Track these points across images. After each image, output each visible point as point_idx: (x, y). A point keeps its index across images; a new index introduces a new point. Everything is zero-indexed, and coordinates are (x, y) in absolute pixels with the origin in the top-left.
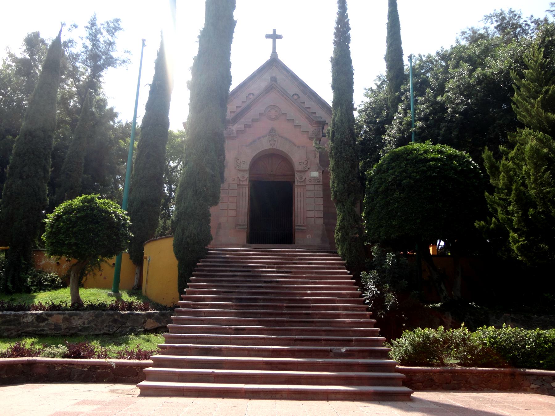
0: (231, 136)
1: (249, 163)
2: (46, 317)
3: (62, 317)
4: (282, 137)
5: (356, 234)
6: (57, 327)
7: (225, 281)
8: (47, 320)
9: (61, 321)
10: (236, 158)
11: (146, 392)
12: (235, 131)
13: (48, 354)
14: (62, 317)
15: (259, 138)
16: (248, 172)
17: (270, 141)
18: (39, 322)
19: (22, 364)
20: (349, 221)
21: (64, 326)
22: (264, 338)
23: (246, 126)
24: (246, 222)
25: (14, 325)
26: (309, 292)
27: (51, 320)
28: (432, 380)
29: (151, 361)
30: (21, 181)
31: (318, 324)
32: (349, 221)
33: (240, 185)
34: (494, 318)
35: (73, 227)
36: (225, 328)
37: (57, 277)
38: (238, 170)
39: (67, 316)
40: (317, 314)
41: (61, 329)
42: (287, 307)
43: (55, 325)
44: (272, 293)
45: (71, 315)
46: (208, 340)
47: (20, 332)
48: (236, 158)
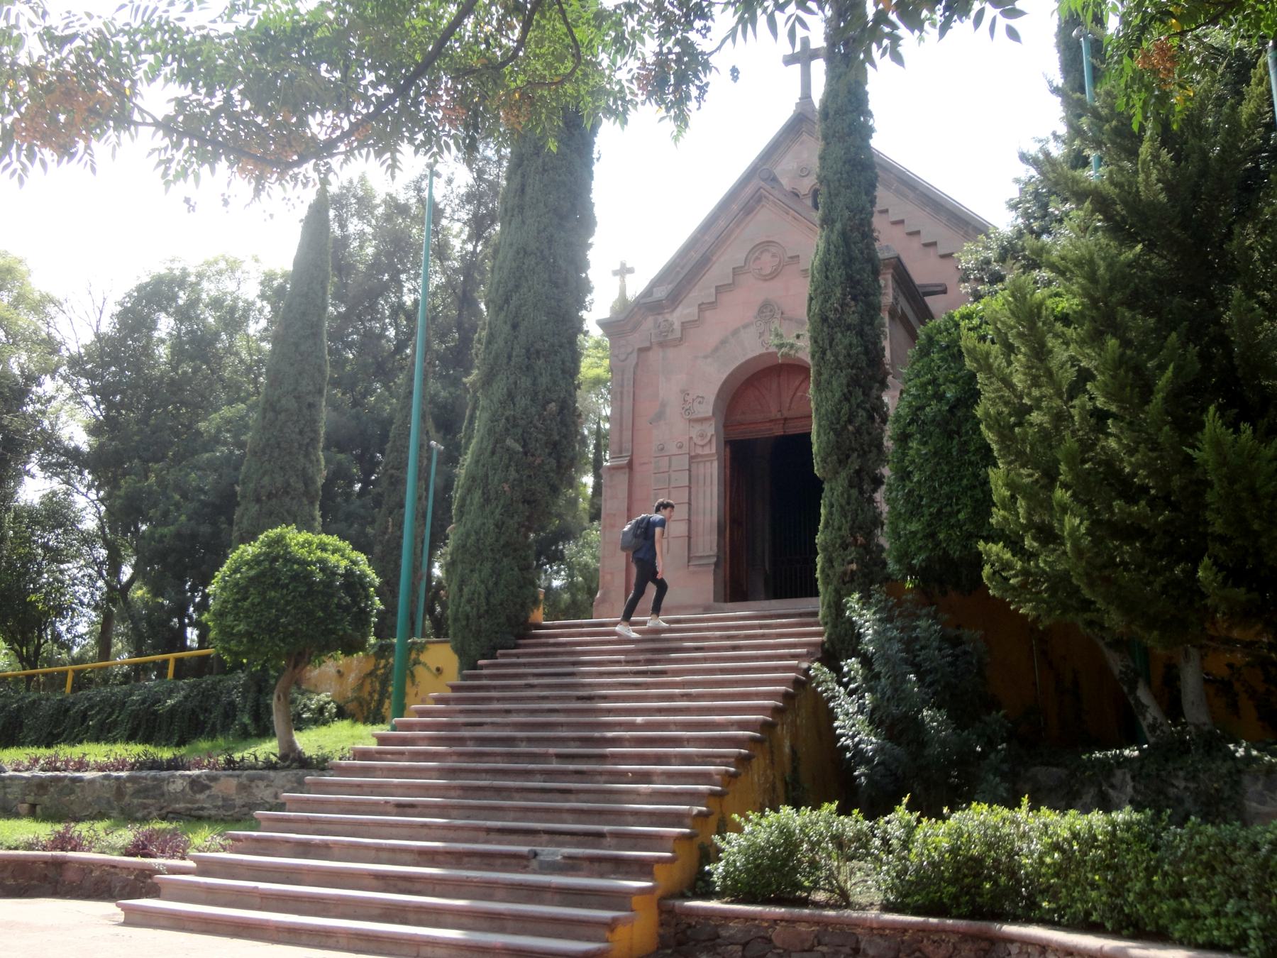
0: (670, 337)
1: (711, 398)
2: (207, 782)
3: (234, 782)
4: (790, 319)
5: (851, 562)
6: (227, 803)
7: (499, 700)
8: (209, 787)
9: (233, 791)
10: (682, 391)
11: (135, 919)
12: (677, 326)
13: (107, 847)
14: (234, 782)
15: (735, 332)
16: (713, 422)
17: (761, 334)
18: (195, 792)
19: (45, 863)
20: (840, 529)
21: (239, 802)
22: (424, 825)
23: (702, 308)
24: (715, 549)
25: (154, 798)
26: (639, 719)
27: (216, 789)
28: (769, 940)
29: (189, 864)
30: (257, 507)
31: (582, 796)
32: (840, 529)
33: (697, 456)
34: (1259, 786)
35: (245, 599)
36: (376, 803)
37: (329, 703)
38: (690, 421)
39: (245, 782)
40: (601, 773)
41: (234, 807)
42: (560, 756)
43: (224, 799)
44: (562, 725)
45: (252, 779)
46: (326, 827)
47: (164, 812)
48: (682, 391)
